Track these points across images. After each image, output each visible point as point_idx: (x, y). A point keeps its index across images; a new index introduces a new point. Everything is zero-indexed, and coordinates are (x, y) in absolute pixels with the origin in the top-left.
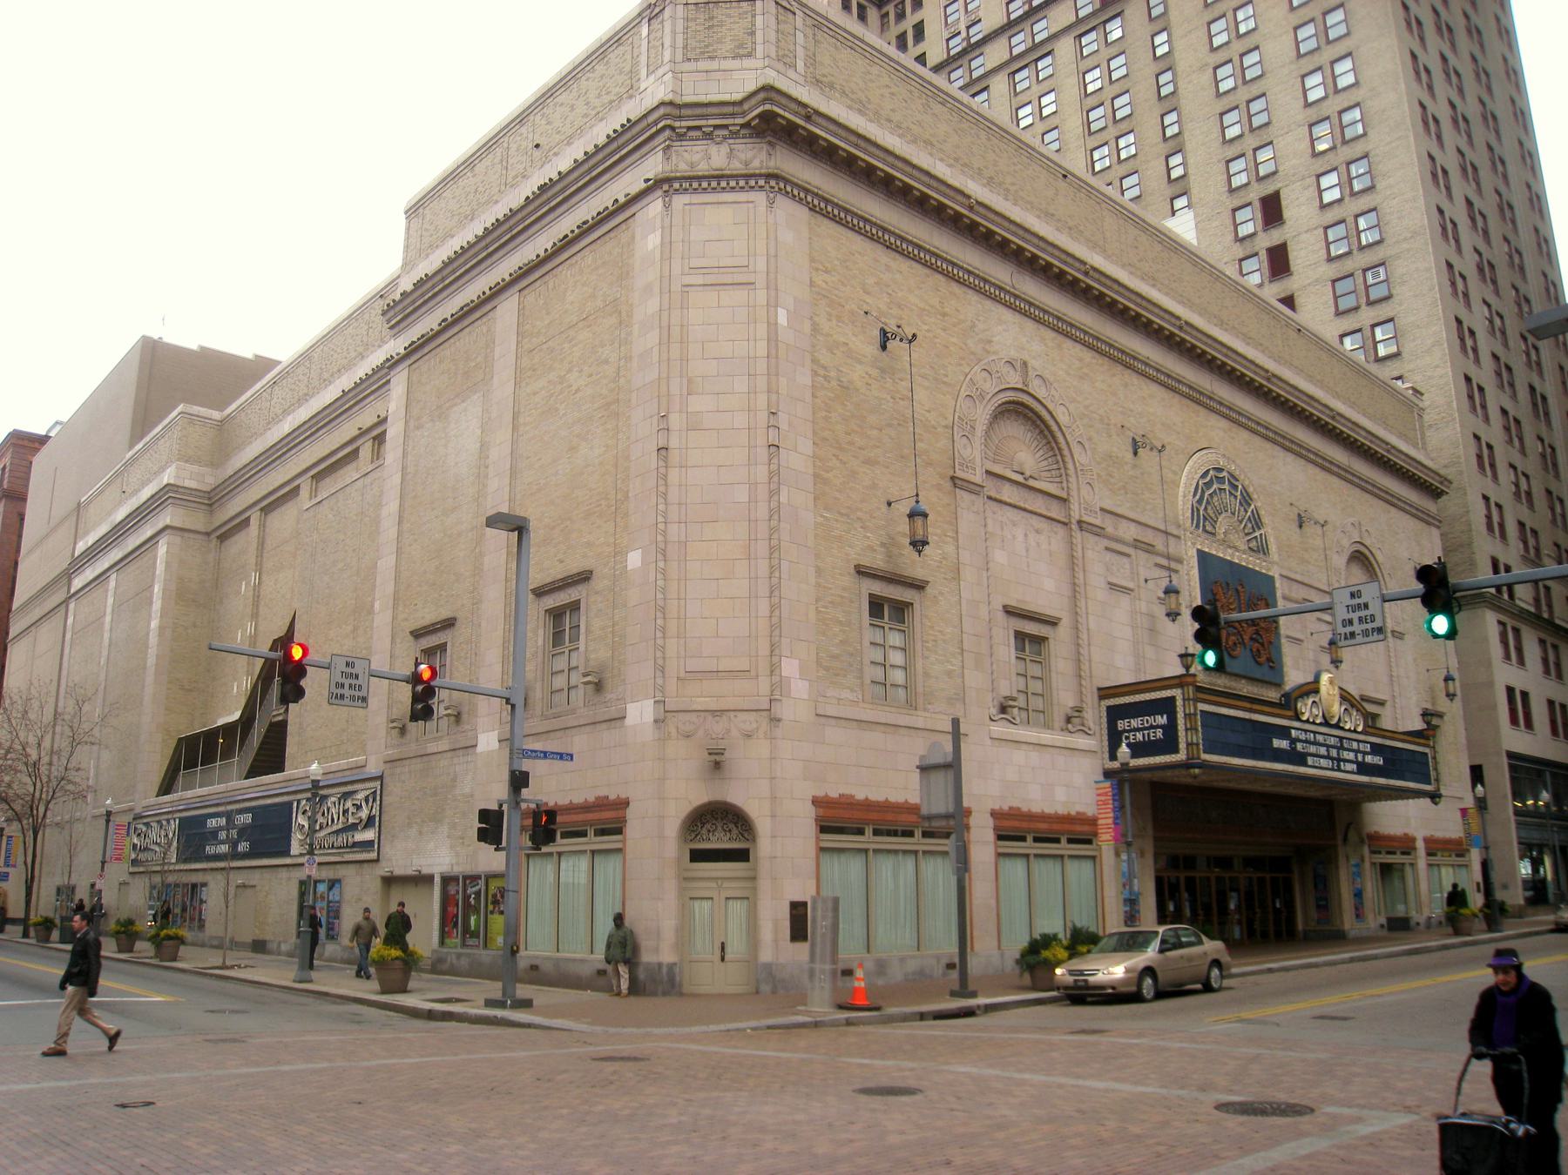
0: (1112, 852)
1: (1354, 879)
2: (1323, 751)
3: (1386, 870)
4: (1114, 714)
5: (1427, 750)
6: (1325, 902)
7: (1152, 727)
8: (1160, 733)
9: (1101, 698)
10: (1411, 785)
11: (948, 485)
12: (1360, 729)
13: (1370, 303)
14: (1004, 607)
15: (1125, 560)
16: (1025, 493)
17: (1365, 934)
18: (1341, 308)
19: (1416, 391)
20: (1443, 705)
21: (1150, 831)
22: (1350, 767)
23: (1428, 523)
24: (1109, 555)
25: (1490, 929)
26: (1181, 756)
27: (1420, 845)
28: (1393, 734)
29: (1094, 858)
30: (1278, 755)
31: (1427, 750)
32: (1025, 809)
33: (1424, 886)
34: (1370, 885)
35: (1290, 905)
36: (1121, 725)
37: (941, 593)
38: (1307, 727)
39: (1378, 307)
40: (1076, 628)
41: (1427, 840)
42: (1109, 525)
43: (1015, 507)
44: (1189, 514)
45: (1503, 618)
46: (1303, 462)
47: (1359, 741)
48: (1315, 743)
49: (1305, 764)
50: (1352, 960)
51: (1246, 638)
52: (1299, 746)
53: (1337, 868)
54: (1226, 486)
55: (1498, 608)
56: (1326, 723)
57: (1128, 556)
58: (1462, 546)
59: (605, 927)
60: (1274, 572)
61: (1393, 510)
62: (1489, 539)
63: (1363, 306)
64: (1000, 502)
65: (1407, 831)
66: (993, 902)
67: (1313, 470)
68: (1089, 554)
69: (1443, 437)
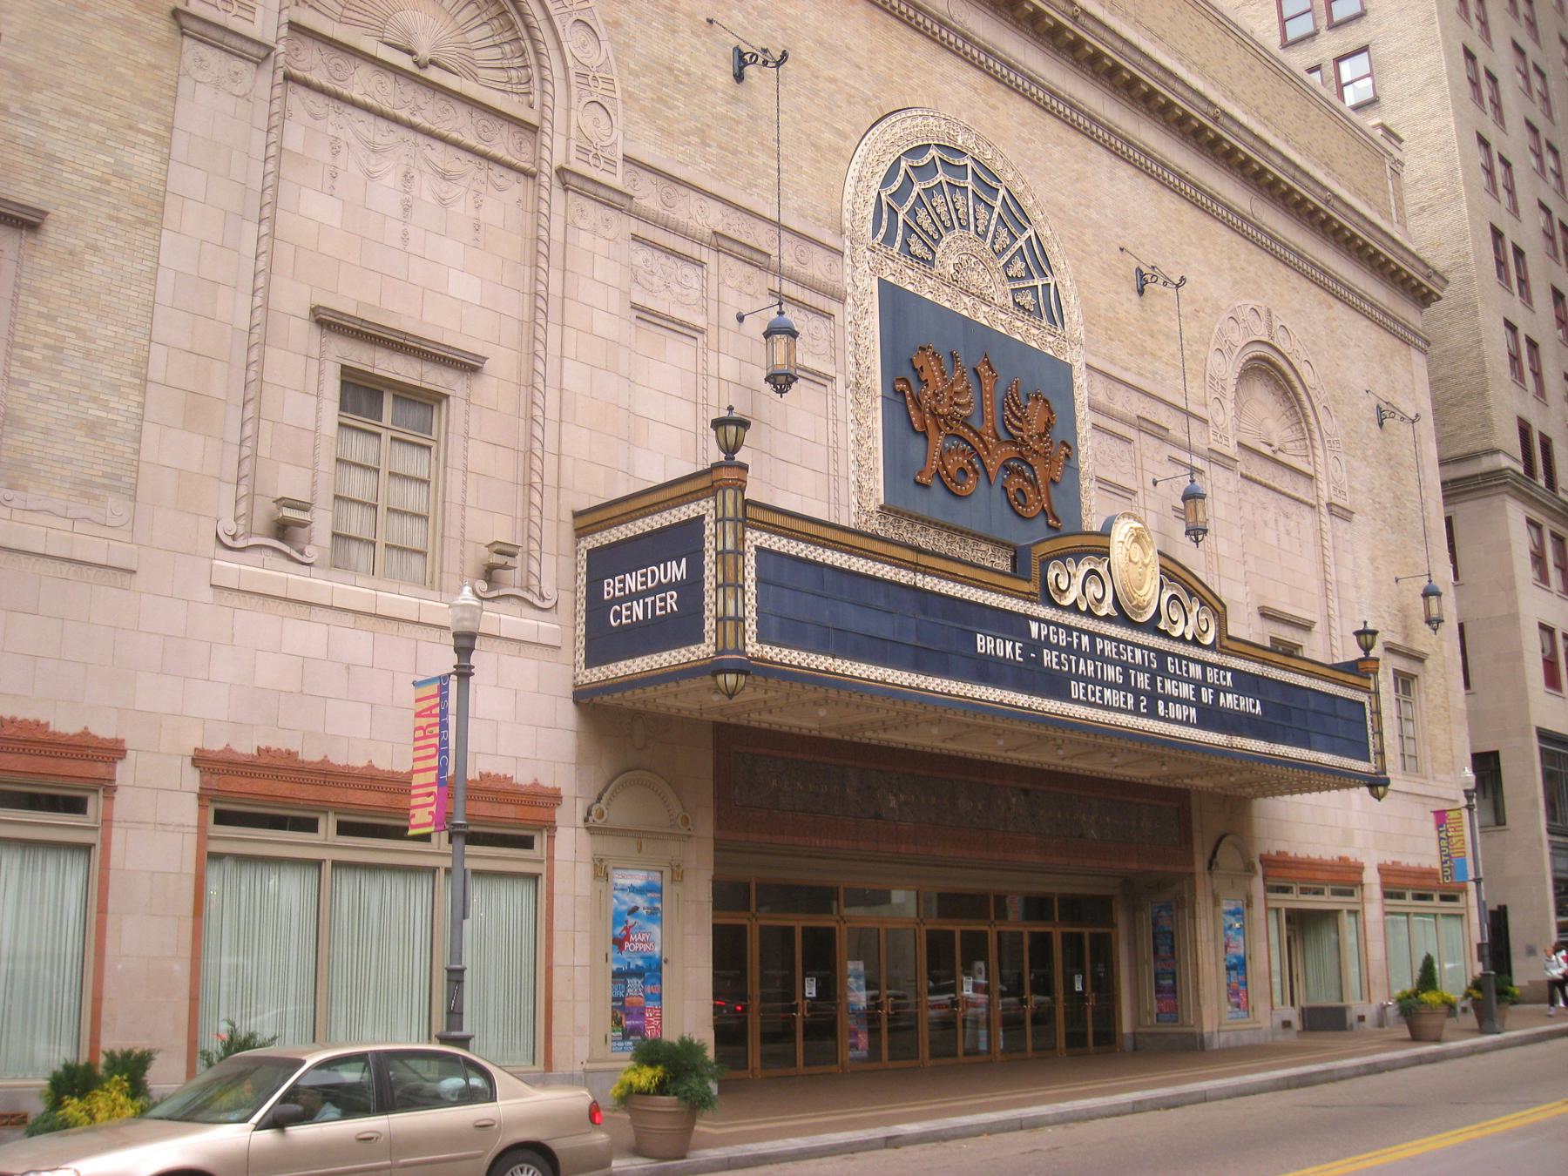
0: (585, 870)
1: (1233, 938)
2: (1112, 673)
3: (1302, 925)
4: (603, 563)
5: (1363, 697)
6: (1170, 983)
7: (661, 588)
8: (672, 600)
9: (581, 533)
10: (1325, 758)
11: (162, 28)
12: (1208, 640)
13: (1334, 26)
14: (315, 310)
15: (688, 270)
16: (421, 97)
17: (1246, 1038)
18: (1291, 36)
19: (1388, 132)
20: (1423, 639)
21: (705, 827)
22: (1177, 711)
23: (1407, 343)
24: (642, 255)
25: (1483, 1030)
26: (704, 650)
27: (1371, 878)
28: (1314, 669)
29: (535, 877)
30: (988, 671)
31: (1363, 697)
32: (311, 754)
33: (1376, 950)
34: (1266, 946)
35: (1105, 987)
36: (611, 588)
37: (94, 248)
38: (1072, 619)
39: (1346, 30)
40: (530, 385)
41: (1383, 870)
42: (648, 195)
43: (382, 115)
44: (870, 210)
45: (1537, 516)
46: (1153, 185)
47: (1205, 664)
48: (1093, 655)
49: (1065, 696)
50: (1138, 1107)
51: (993, 465)
52: (1049, 658)
53: (1193, 916)
54: (969, 183)
55: (1528, 499)
56: (1122, 617)
57: (701, 264)
58: (1469, 396)
59: (1419, 964)
60: (1076, 358)
61: (1338, 306)
62: (1515, 389)
63: (1323, 32)
64: (338, 97)
65: (1344, 853)
66: (181, 969)
67: (1169, 200)
68: (585, 239)
69: (1436, 205)
